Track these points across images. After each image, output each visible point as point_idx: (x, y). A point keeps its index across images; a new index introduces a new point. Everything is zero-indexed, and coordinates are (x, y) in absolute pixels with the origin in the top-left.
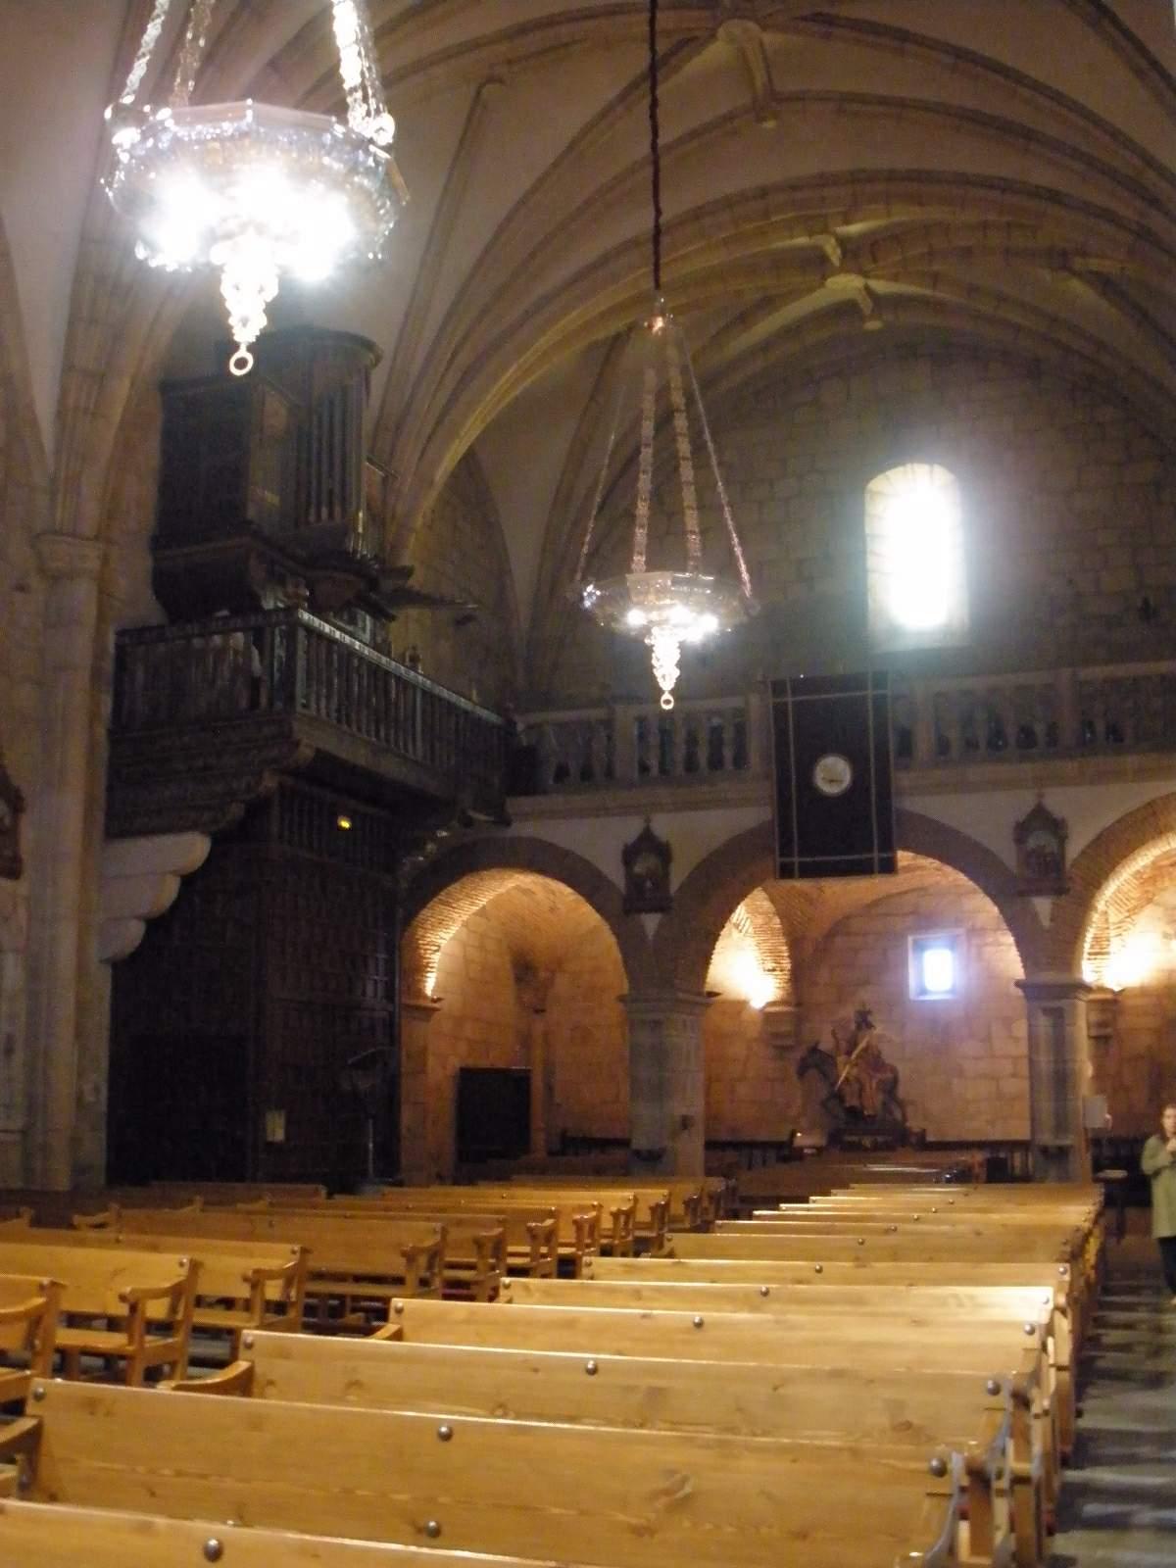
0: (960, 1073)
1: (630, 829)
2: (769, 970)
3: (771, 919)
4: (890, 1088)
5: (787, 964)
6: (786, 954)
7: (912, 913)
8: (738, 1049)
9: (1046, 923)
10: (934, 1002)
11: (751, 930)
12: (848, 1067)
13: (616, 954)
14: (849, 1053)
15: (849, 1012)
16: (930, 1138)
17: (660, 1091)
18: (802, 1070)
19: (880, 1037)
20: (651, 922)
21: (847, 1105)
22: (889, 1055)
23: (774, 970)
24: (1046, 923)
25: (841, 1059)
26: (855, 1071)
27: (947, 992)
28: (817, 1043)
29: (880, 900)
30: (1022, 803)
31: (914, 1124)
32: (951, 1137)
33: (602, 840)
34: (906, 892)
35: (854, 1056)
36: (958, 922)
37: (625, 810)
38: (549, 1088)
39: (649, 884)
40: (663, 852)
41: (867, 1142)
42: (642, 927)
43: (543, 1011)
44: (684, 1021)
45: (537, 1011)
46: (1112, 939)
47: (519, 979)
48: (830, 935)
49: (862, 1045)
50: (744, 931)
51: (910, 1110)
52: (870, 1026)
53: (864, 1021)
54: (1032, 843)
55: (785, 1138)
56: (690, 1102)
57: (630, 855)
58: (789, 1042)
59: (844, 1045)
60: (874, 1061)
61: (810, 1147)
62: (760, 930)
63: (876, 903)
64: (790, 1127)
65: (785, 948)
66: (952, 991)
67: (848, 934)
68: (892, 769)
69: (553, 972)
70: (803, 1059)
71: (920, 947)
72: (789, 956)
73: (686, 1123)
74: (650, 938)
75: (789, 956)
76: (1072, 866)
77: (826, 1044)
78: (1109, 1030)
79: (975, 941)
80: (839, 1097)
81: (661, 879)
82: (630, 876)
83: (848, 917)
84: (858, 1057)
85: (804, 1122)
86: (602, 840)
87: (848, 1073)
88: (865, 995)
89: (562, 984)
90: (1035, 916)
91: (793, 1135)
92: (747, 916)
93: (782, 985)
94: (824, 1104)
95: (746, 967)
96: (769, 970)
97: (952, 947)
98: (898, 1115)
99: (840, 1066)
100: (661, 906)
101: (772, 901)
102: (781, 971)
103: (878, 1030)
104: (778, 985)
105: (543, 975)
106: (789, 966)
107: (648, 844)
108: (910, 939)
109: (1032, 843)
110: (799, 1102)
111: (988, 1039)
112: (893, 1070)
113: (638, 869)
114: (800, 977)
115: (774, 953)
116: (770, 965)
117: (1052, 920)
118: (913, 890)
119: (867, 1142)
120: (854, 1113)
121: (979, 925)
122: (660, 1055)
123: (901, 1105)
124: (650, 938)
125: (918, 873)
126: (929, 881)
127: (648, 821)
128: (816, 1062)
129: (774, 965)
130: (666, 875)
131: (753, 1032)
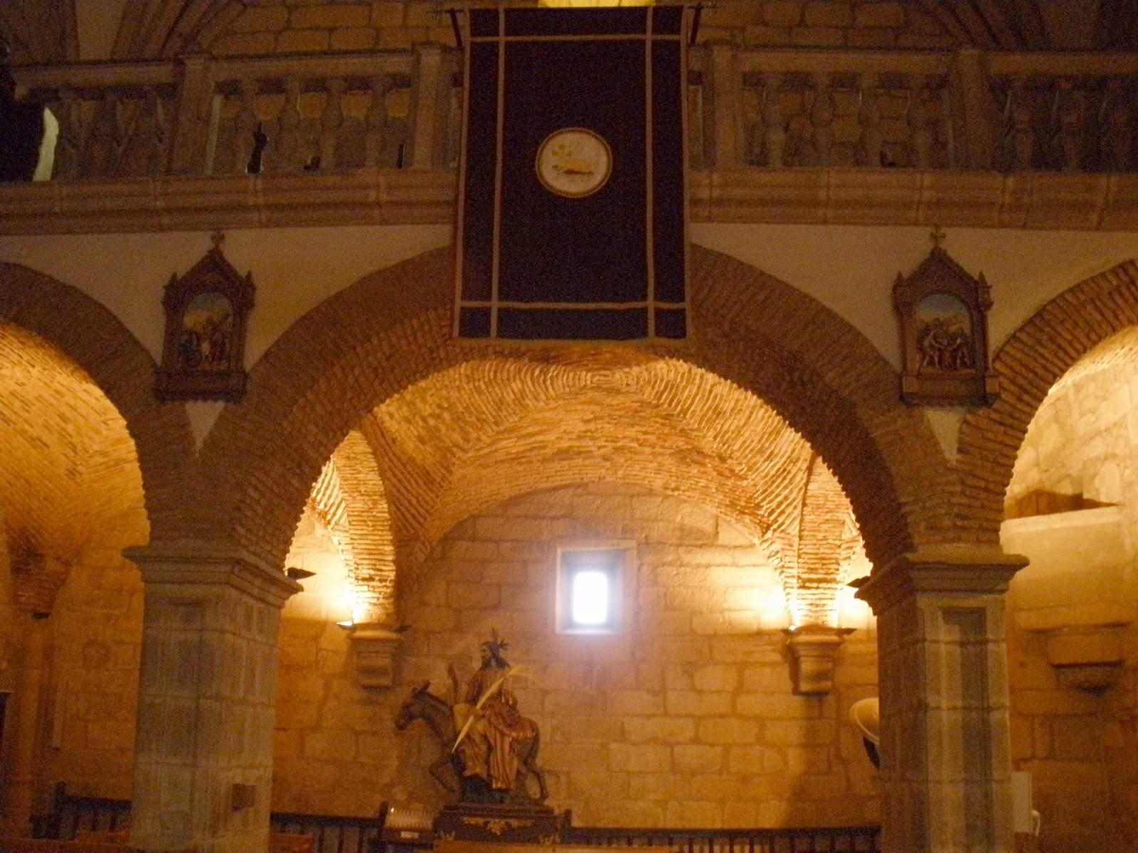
0: (622, 736)
1: (184, 251)
2: (364, 579)
3: (375, 503)
4: (527, 753)
5: (390, 572)
6: (391, 558)
7: (564, 516)
8: (312, 686)
9: (952, 455)
10: (579, 636)
11: (344, 520)
12: (471, 719)
13: (129, 448)
14: (474, 701)
15: (470, 647)
16: (576, 823)
17: (193, 732)
18: (405, 718)
19: (516, 679)
20: (203, 417)
21: (468, 773)
22: (527, 707)
23: (371, 579)
24: (952, 455)
25: (460, 708)
26: (480, 726)
27: (599, 627)
28: (427, 685)
29: (522, 496)
30: (907, 247)
31: (556, 803)
32: (606, 822)
33: (131, 274)
34: (556, 489)
35: (479, 705)
36: (627, 532)
37: (182, 217)
38: (46, 727)
39: (206, 347)
40: (240, 292)
41: (496, 826)
42: (185, 425)
43: (46, 615)
44: (249, 611)
45: (39, 616)
46: (842, 563)
47: (17, 569)
48: (447, 540)
49: (493, 689)
50: (333, 523)
51: (550, 781)
52: (502, 664)
53: (494, 658)
54: (926, 313)
55: (371, 813)
56: (250, 762)
57: (177, 295)
58: (385, 681)
59: (464, 688)
60: (506, 712)
61: (411, 829)
62: (358, 519)
63: (514, 501)
64: (377, 800)
65: (389, 548)
66: (608, 625)
67: (474, 539)
68: (686, 164)
69: (67, 564)
70: (406, 706)
71: (571, 567)
72: (394, 561)
73: (241, 797)
74: (199, 444)
75: (394, 561)
76: (997, 357)
77: (439, 683)
78: (827, 685)
79: (648, 559)
80: (457, 761)
81: (228, 340)
82: (173, 331)
83: (475, 517)
84: (483, 708)
85: (399, 794)
86: (131, 274)
87: (471, 728)
88: (491, 622)
89: (78, 581)
90: (930, 441)
91: (383, 813)
92: (341, 495)
93: (381, 601)
94: (433, 771)
95: (337, 579)
96: (364, 579)
97: (611, 568)
98: (533, 790)
99: (459, 719)
100: (228, 385)
101: (382, 474)
102: (381, 581)
103: (514, 670)
104: (374, 601)
105: (51, 565)
106: (392, 575)
107: (217, 277)
108: (559, 551)
109: (926, 313)
110: (394, 763)
111: (661, 692)
112: (534, 728)
113: (193, 319)
114: (406, 590)
115: (374, 555)
116: (365, 572)
117: (960, 451)
118: (566, 487)
119: (496, 826)
120: (478, 787)
121: (655, 535)
122: (199, 666)
123: (538, 776)
124: (199, 444)
125: (579, 461)
126: (591, 475)
127: (219, 239)
128: (424, 711)
129: (372, 572)
130: (240, 332)
131: (335, 663)
